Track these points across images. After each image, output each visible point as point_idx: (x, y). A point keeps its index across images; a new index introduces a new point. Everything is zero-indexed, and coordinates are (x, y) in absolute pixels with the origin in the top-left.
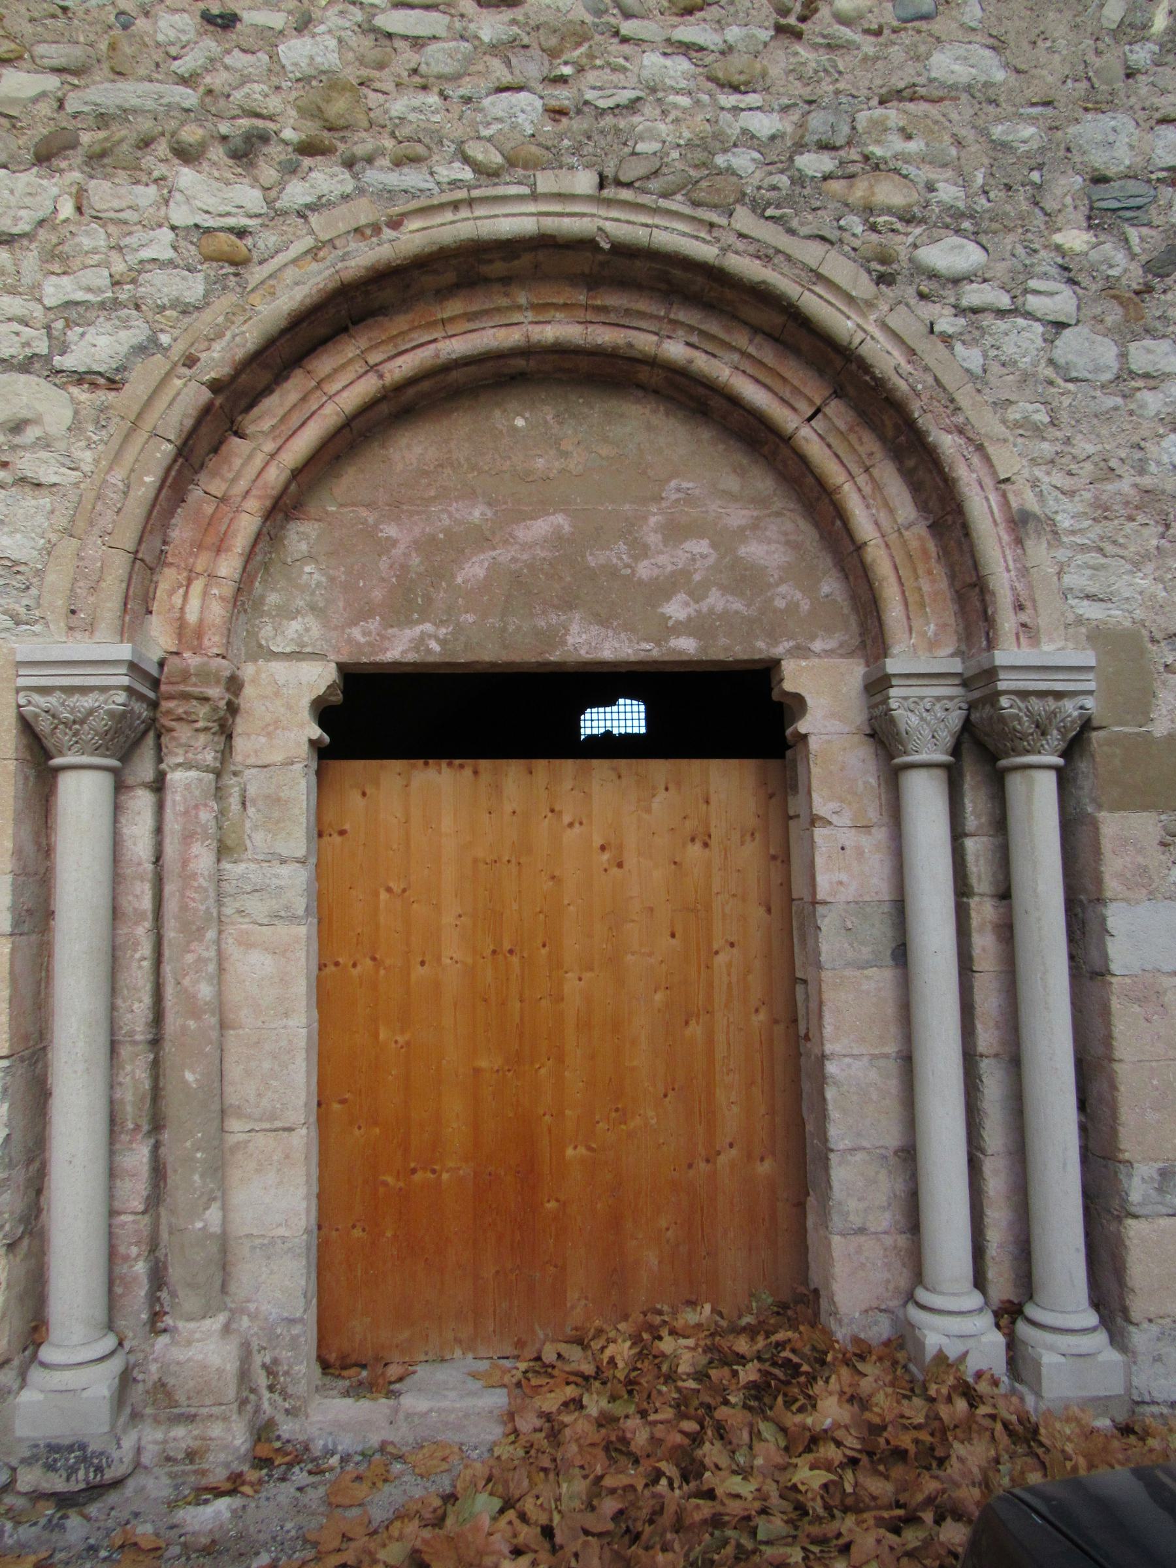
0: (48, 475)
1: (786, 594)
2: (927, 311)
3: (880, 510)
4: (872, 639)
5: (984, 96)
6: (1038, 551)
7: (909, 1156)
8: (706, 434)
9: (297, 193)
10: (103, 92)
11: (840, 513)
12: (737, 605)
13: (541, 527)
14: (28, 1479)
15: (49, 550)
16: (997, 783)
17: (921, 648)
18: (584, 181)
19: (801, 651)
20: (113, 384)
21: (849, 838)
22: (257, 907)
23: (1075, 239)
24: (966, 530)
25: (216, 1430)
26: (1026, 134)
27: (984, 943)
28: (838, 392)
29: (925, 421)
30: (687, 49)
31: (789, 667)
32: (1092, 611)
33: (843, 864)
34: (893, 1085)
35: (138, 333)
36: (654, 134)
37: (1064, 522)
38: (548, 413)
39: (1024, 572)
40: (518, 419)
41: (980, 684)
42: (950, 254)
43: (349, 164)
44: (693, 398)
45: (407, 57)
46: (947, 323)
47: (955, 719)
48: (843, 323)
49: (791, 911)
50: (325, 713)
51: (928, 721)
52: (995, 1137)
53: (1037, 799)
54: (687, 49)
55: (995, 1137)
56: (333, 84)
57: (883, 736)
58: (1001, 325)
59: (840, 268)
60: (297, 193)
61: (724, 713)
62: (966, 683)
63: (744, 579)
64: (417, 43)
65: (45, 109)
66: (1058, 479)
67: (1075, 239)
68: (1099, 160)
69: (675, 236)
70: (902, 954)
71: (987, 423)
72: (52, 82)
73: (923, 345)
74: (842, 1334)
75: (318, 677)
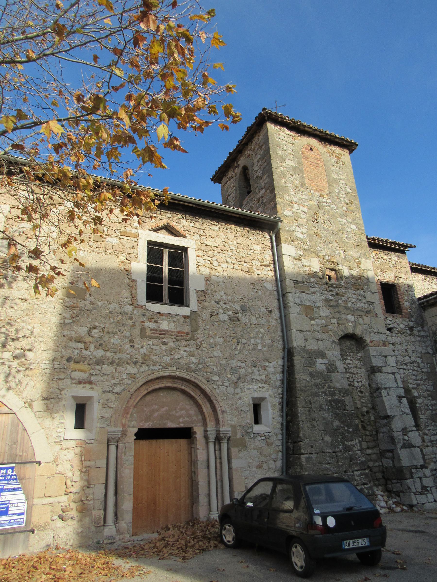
0: (112, 406)
1: (194, 418)
2: (212, 385)
3: (207, 408)
4: (205, 424)
5: (219, 357)
6: (225, 415)
7: (209, 495)
8: (185, 396)
9: (142, 369)
10: (118, 355)
11: (202, 408)
12: (188, 419)
13: (164, 409)
14: (105, 541)
15: (112, 416)
16: (220, 444)
17: (211, 427)
18: (175, 368)
19: (196, 426)
20: (120, 394)
21: (202, 451)
22: (127, 463)
23: (229, 376)
24: (217, 412)
25: (126, 535)
26: (224, 362)
27: (218, 465)
28: (202, 393)
29: (212, 399)
30: (186, 351)
31: (194, 428)
32: (231, 423)
33: (201, 455)
34: (207, 485)
35: (122, 388)
36: (183, 362)
37: (228, 412)
38: (165, 393)
39: (223, 418)
40: (162, 394)
41: (218, 432)
42: (215, 378)
43: (147, 365)
44: (184, 392)
45: (155, 352)
46: (215, 387)
47: (215, 436)
48: (204, 387)
49: (193, 462)
50: (136, 435)
51: (212, 436)
52: (219, 491)
53: (224, 446)
54: (186, 351)
55: (219, 491)
56: (146, 355)
57: (206, 438)
58: (221, 387)
59: (204, 380)
60: (142, 369)
61: (185, 433)
62: (216, 431)
63: (189, 416)
64: (156, 350)
65: (111, 357)
66: (227, 406)
67: (229, 376)
68: (232, 366)
69: (185, 375)
70: (208, 467)
71: (219, 399)
72: (112, 354)
73: (212, 390)
74: (201, 520)
75: (136, 430)
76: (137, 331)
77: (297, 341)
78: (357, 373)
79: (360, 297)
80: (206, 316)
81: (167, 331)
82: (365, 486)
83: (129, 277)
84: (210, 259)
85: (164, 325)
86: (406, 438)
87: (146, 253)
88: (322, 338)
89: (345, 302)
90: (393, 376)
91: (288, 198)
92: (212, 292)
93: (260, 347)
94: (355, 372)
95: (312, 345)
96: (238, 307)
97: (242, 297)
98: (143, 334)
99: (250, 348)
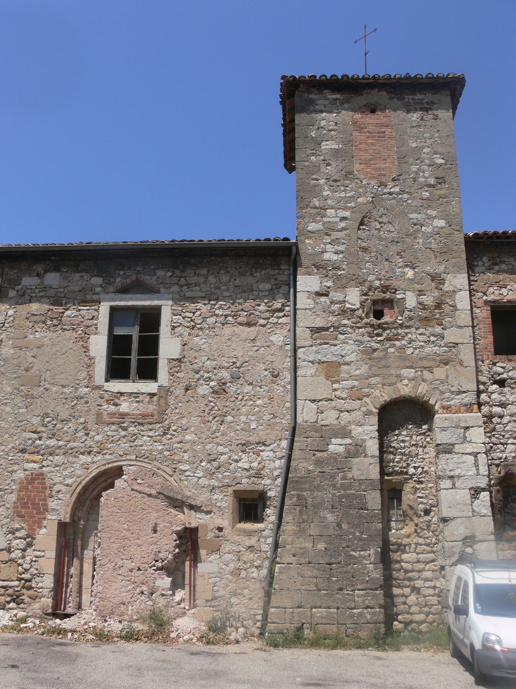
18: (134, 457)
76: (92, 418)
77: (307, 413)
78: (417, 455)
79: (432, 339)
80: (179, 391)
81: (127, 414)
82: (369, 610)
83: (87, 354)
84: (191, 315)
85: (125, 407)
86: (469, 550)
87: (108, 322)
88: (349, 408)
89: (402, 348)
90: (472, 458)
91: (317, 204)
92: (190, 359)
93: (253, 426)
94: (413, 453)
95: (330, 417)
96: (225, 374)
97: (234, 360)
98: (99, 419)
99: (238, 427)
